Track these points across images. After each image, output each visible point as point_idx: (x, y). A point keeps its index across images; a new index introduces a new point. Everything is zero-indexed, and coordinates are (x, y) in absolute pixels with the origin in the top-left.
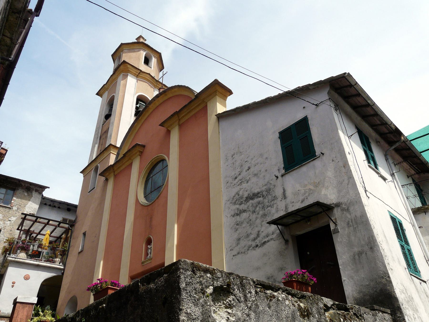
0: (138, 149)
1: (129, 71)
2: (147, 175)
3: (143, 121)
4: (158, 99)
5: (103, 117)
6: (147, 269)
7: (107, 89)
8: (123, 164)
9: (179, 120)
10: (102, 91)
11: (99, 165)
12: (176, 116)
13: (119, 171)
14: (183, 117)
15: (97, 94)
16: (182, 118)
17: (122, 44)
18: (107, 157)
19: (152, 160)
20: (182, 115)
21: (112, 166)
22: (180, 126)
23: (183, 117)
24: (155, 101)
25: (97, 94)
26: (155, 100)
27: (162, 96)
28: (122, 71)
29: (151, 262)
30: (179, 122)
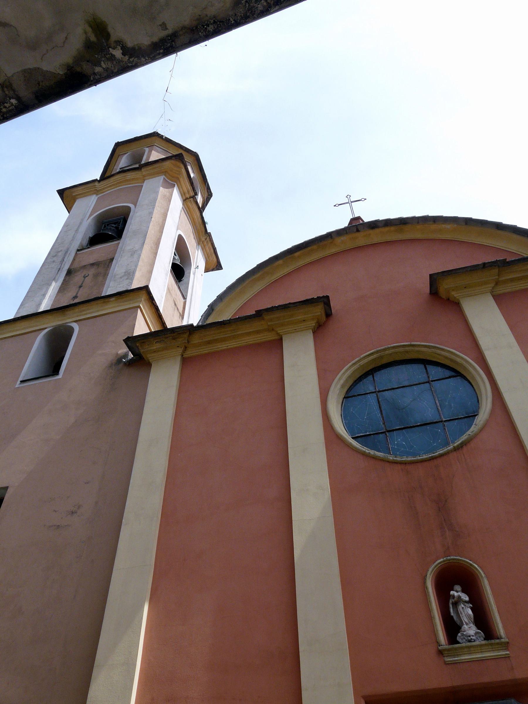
0: (319, 310)
1: (178, 179)
2: (351, 382)
3: (112, 306)
4: (371, 231)
5: (132, 225)
6: (486, 679)
7: (97, 192)
8: (234, 337)
9: (497, 283)
10: (79, 190)
11: (76, 327)
12: (496, 271)
13: (205, 350)
14: (512, 280)
15: (61, 193)
16: (505, 282)
17: (155, 135)
18: (37, 332)
19: (385, 350)
20: (511, 276)
21: (190, 328)
22: (185, 361)
23: (512, 280)
24: (358, 234)
25: (61, 193)
26: (358, 231)
27: (387, 229)
28: (165, 173)
29: (507, 657)
30: (493, 288)
